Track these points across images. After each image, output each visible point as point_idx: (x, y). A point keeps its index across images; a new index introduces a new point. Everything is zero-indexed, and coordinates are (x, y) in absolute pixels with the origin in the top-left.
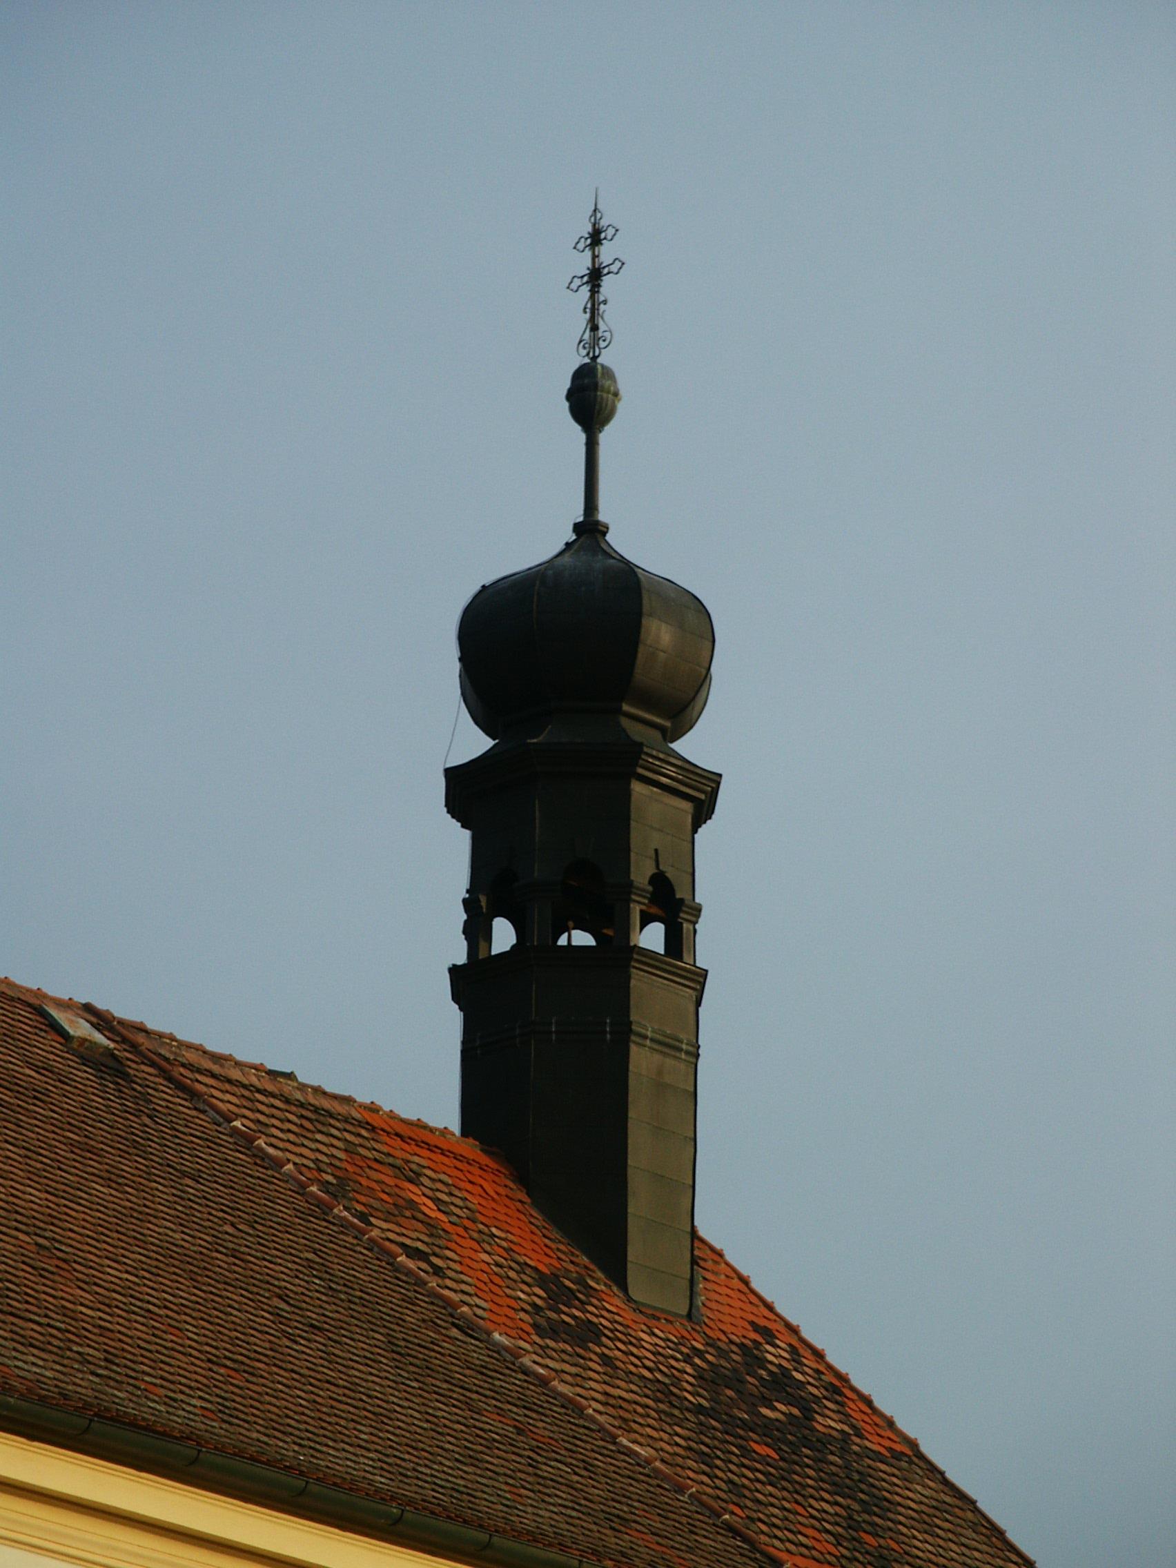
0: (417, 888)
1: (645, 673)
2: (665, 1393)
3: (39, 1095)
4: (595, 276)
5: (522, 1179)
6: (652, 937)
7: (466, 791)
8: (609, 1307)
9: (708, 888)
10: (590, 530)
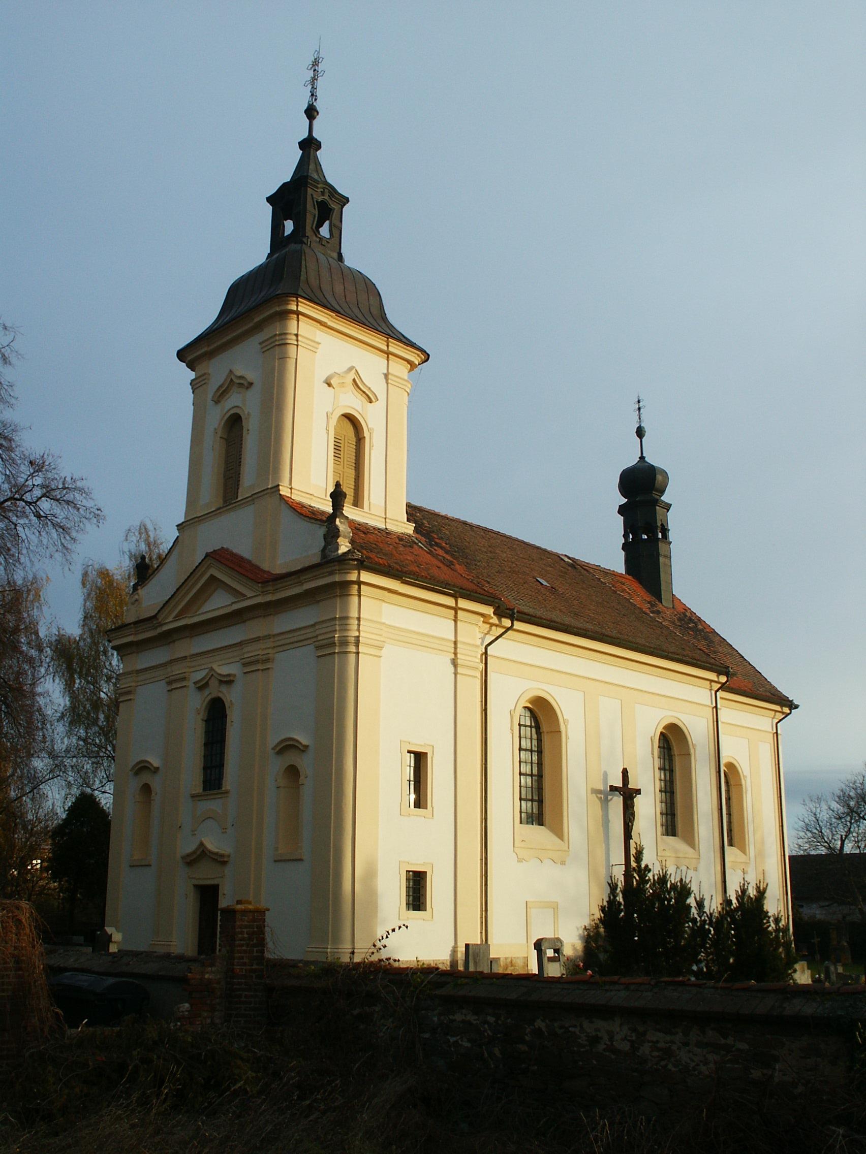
0: (614, 529)
1: (657, 485)
2: (673, 622)
3: (566, 573)
4: (639, 409)
5: (641, 583)
6: (660, 536)
7: (622, 510)
8: (660, 607)
9: (671, 526)
10: (642, 458)
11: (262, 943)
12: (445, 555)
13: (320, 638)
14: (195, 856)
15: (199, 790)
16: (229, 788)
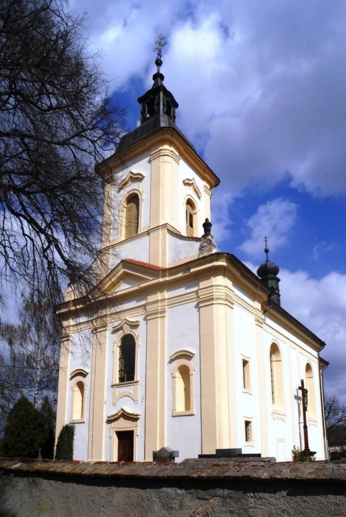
11: (288, 462)
12: (49, 323)
13: (200, 297)
14: (117, 416)
15: (117, 382)
16: (138, 379)
